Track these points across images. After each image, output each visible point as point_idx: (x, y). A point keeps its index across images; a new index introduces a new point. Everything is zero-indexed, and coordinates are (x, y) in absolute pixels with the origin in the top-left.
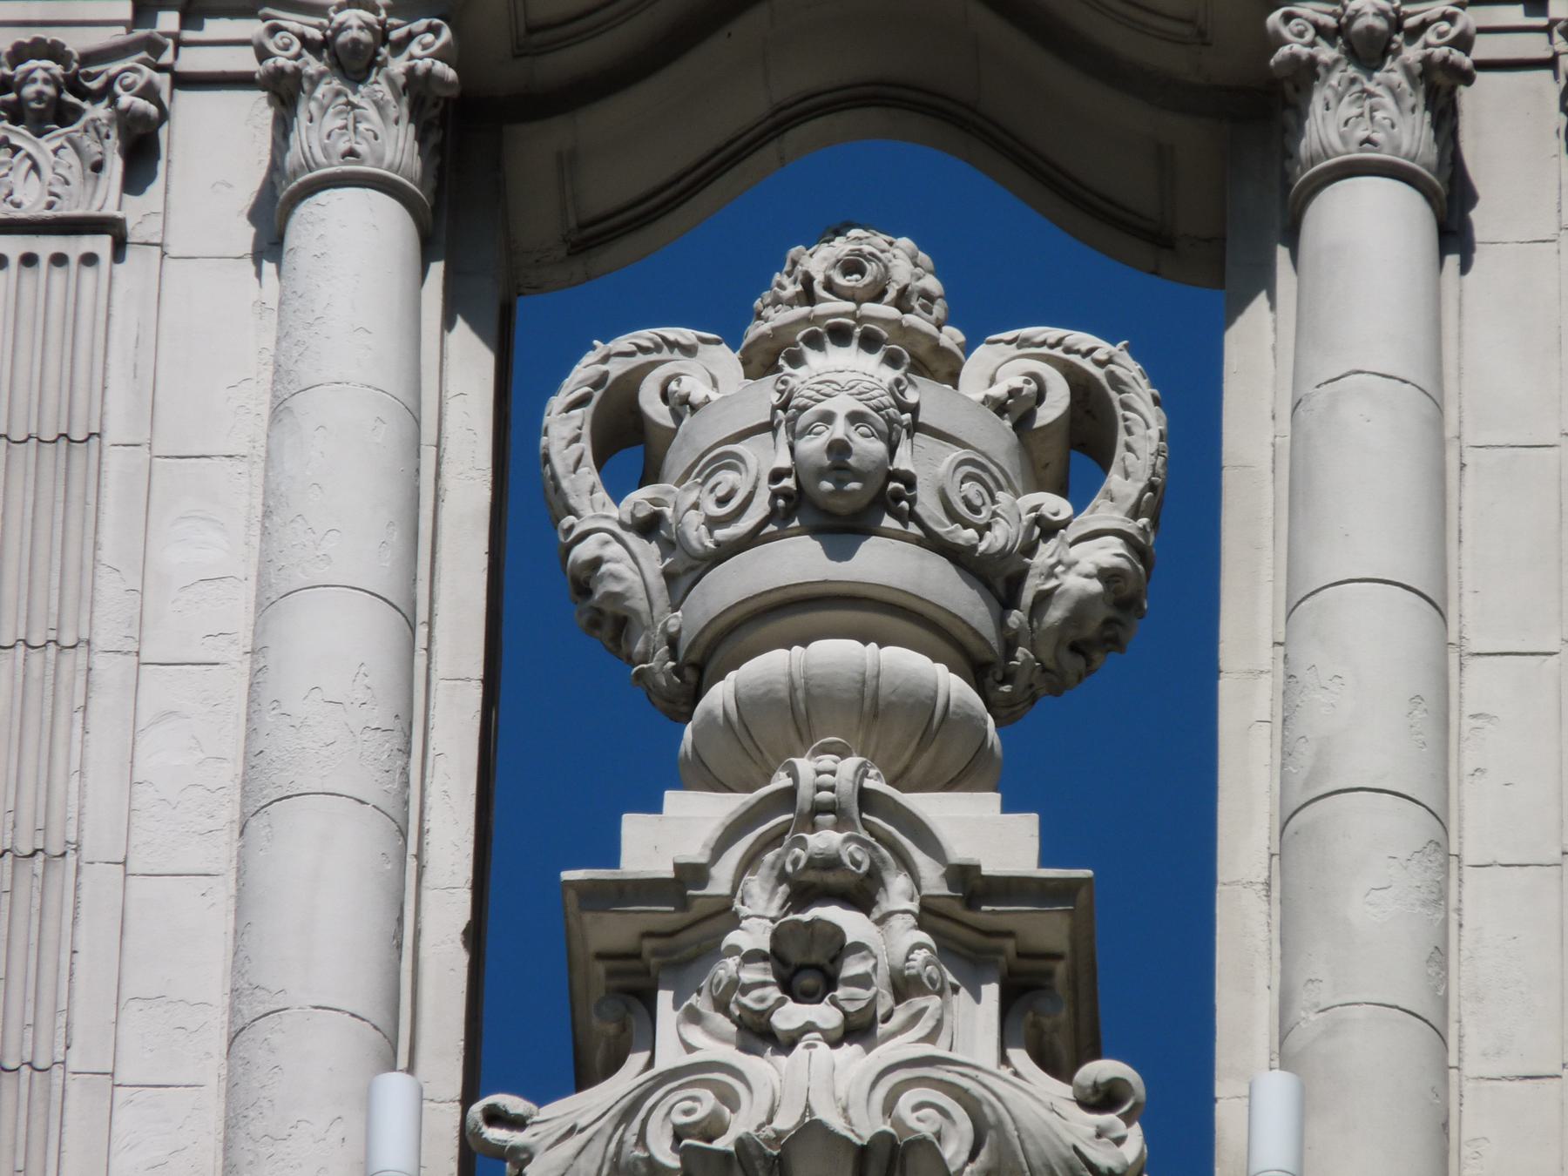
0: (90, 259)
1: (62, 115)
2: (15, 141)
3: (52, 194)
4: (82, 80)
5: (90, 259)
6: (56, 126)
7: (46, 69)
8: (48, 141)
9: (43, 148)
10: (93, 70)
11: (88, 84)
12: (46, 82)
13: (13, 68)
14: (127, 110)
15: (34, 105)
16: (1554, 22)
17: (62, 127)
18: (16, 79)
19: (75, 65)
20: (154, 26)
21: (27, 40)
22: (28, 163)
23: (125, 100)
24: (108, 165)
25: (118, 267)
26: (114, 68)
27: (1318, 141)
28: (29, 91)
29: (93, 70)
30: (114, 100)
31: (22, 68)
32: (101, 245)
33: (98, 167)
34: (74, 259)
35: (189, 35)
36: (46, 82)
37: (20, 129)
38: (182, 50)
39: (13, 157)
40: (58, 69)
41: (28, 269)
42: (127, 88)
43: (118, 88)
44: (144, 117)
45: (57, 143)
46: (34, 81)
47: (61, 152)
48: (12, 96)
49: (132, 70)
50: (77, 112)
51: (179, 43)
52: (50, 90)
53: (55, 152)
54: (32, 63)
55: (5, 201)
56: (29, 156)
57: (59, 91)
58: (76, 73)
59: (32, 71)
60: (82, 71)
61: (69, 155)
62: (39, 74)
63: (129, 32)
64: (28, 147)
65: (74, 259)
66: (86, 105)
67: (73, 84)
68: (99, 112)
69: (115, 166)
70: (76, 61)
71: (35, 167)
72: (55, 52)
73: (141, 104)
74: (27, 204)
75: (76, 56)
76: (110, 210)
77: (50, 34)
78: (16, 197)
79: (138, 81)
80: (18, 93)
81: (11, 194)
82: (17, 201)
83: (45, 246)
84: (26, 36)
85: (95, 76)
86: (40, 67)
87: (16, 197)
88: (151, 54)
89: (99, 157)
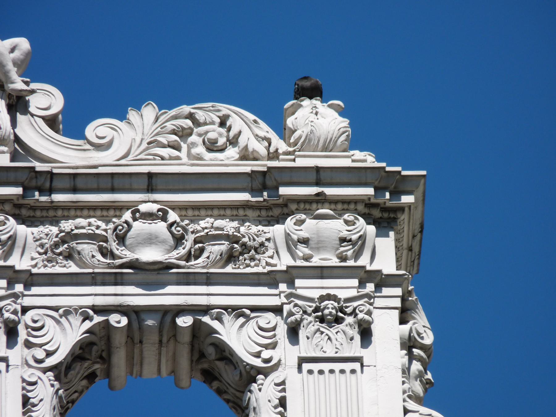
0: (353, 371)
1: (338, 320)
2: (322, 329)
3: (337, 348)
4: (344, 308)
5: (353, 371)
6: (336, 324)
7: (332, 304)
8: (333, 329)
9: (332, 332)
10: (348, 305)
11: (346, 310)
12: (332, 308)
13: (320, 304)
14: (361, 320)
15: (329, 317)
16: (281, 292)
17: (338, 324)
18: (322, 308)
19: (342, 303)
20: (14, 289)
21: (324, 294)
22: (327, 337)
23: (361, 316)
24: (355, 338)
25: (7, 374)
26: (355, 304)
27: (74, 332)
28: (326, 312)
29: (348, 305)
30: (356, 315)
31: (322, 304)
32: (356, 366)
33: (352, 339)
34: (348, 371)
35: (26, 293)
36: (332, 308)
37: (323, 325)
38: (24, 298)
39: (321, 335)
40: (336, 304)
41: (311, 375)
42: (7, 311)
43: (357, 311)
44: (14, 321)
45: (336, 330)
46: (328, 308)
47: (338, 333)
48: (320, 314)
49: (361, 305)
50: (343, 319)
51: (24, 295)
52: (334, 312)
53: (337, 333)
54: (326, 302)
55: (321, 351)
56: (327, 335)
57: (337, 312)
58: (342, 306)
59: (327, 305)
60: (344, 305)
61: (340, 336)
62: (330, 306)
63: (6, 292)
64: (326, 331)
65: (348, 371)
66: (346, 317)
67: (341, 310)
68: (350, 320)
69: (358, 338)
70: (343, 301)
71: (329, 338)
72: (335, 298)
73: (13, 317)
74: (328, 352)
75: (343, 300)
76: (357, 355)
77: (332, 292)
78: (324, 349)
79: (365, 309)
80: (322, 312)
81: (322, 348)
82: (325, 351)
83: (326, 366)
84: (324, 292)
85: (349, 307)
86: (330, 304)
87: (324, 349)
88: (15, 299)
89: (352, 335)
